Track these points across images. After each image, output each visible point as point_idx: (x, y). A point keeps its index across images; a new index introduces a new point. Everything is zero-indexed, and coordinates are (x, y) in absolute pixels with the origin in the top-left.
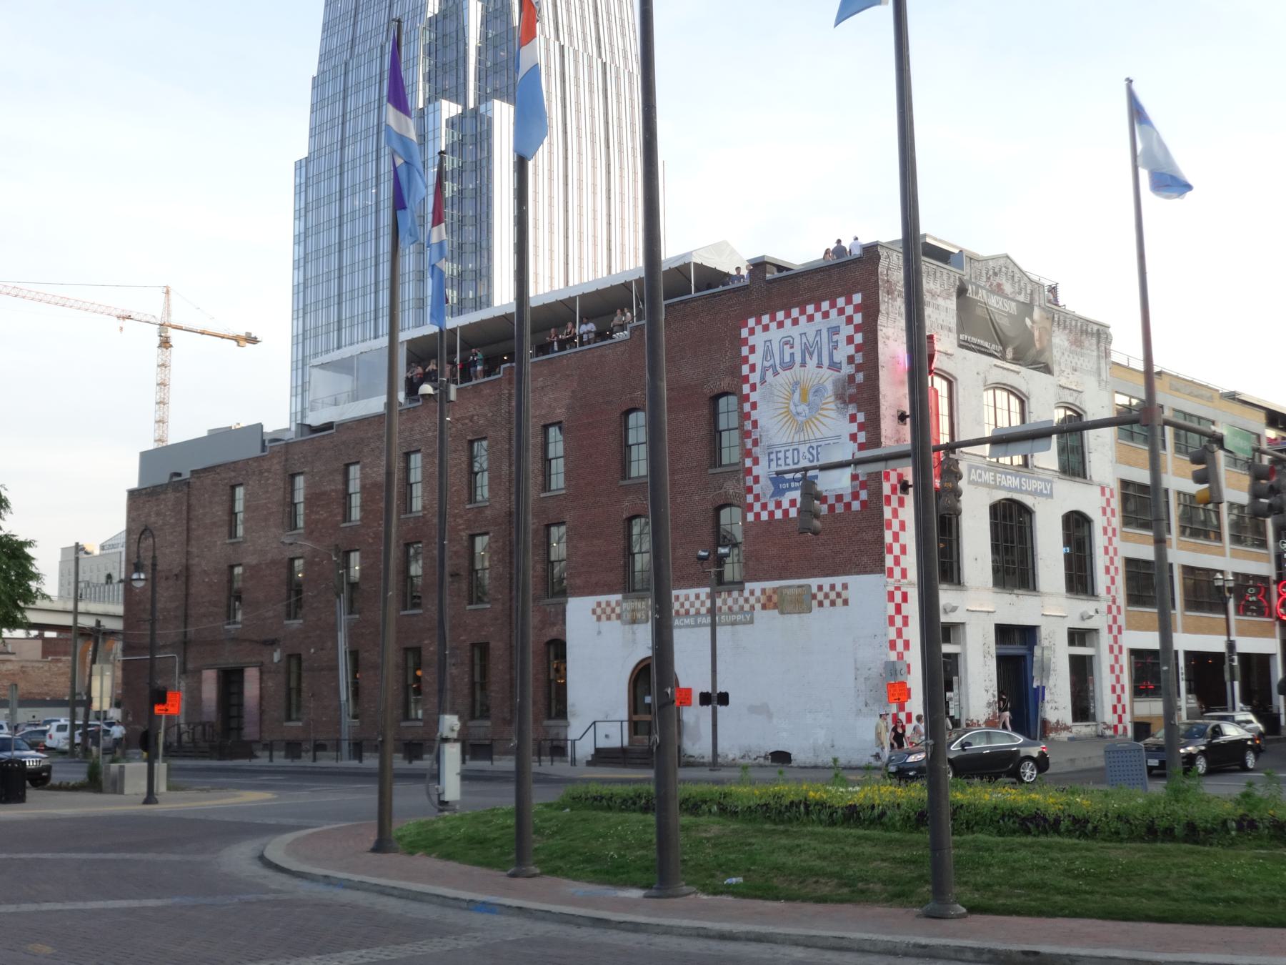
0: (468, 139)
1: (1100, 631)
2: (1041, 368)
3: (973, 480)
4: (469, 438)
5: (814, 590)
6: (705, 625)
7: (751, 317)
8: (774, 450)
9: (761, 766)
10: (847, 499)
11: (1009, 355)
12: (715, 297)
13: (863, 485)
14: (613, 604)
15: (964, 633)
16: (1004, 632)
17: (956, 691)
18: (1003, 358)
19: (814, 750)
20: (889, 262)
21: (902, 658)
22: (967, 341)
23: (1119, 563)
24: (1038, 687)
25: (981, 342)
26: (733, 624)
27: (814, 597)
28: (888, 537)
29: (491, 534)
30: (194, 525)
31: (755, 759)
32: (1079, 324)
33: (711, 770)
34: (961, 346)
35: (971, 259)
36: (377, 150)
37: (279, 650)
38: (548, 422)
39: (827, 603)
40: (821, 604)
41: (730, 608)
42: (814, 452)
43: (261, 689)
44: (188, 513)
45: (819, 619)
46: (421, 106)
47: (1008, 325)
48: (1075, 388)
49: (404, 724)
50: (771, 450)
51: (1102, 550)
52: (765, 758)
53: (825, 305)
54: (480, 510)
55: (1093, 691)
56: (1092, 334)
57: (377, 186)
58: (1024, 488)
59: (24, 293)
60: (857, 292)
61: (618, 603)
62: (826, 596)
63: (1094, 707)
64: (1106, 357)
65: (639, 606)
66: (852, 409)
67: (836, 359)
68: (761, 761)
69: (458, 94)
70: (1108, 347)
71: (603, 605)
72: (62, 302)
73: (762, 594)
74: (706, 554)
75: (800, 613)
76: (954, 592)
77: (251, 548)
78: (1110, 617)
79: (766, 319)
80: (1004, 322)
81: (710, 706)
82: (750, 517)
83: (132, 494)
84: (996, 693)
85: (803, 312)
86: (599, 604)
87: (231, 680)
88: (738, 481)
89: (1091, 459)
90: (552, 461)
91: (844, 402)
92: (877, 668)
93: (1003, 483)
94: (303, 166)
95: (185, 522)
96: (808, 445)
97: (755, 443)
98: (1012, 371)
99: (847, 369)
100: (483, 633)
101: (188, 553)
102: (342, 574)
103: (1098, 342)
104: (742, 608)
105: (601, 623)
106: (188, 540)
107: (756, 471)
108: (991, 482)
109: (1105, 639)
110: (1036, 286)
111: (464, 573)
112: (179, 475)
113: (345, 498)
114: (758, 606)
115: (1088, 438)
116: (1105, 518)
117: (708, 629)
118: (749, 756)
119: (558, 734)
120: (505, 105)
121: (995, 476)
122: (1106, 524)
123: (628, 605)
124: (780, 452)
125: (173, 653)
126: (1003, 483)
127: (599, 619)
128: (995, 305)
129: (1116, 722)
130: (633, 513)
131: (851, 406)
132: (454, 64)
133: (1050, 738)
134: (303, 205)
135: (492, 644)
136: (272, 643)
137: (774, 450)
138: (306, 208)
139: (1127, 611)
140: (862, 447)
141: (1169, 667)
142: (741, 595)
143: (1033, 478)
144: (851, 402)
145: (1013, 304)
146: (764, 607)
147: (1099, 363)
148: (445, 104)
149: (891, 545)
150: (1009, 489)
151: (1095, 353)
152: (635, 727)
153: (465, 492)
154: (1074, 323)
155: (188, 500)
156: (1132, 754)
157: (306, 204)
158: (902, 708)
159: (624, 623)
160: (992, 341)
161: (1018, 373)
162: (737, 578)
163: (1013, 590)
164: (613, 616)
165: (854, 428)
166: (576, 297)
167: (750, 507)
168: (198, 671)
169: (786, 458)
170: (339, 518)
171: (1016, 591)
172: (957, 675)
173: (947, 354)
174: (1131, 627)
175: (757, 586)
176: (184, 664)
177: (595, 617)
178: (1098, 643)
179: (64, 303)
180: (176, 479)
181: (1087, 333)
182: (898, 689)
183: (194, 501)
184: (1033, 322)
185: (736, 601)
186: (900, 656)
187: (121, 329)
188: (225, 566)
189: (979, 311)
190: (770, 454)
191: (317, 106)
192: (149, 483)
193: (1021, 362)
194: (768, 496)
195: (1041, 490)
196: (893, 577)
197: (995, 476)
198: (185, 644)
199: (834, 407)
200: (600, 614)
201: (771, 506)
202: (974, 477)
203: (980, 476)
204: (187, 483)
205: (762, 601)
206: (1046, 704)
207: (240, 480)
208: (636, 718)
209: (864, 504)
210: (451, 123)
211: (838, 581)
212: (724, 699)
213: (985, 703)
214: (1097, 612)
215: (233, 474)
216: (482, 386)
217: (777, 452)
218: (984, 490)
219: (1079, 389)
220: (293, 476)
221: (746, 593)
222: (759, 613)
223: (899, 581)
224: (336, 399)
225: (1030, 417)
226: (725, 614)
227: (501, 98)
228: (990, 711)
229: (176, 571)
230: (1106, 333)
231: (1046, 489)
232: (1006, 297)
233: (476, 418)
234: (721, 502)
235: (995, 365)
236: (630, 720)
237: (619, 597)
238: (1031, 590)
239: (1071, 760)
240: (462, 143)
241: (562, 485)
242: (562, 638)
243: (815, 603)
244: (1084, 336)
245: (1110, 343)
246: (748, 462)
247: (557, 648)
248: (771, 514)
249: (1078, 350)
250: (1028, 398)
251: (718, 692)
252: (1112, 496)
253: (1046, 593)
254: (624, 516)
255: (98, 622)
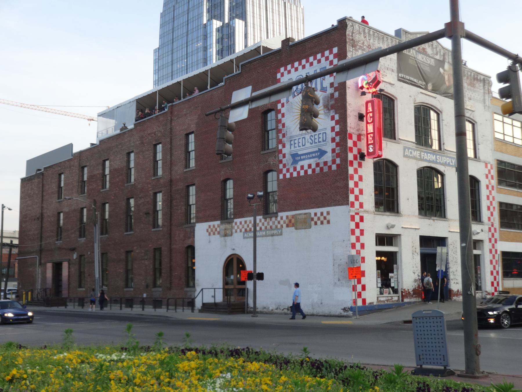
0: (225, 37)
1: (484, 241)
2: (449, 96)
3: (407, 155)
4: (154, 143)
5: (313, 215)
6: (250, 237)
7: (282, 67)
8: (293, 139)
9: (286, 314)
10: (329, 164)
11: (430, 87)
12: (265, 58)
13: (338, 155)
14: (216, 226)
15: (400, 240)
16: (425, 241)
17: (395, 273)
18: (426, 89)
19: (312, 305)
20: (353, 29)
21: (360, 253)
22: (403, 78)
23: (496, 205)
24: (439, 270)
25: (412, 79)
26: (272, 235)
27: (312, 219)
28: (351, 184)
29: (163, 192)
30: (44, 194)
31: (283, 310)
32: (472, 74)
33: (252, 316)
34: (399, 80)
35: (406, 32)
36: (187, 43)
37: (76, 253)
38: (188, 132)
39: (319, 222)
40: (316, 223)
41: (271, 227)
42: (313, 139)
43: (69, 272)
44: (43, 188)
45: (315, 231)
46: (205, 22)
47: (429, 70)
48: (470, 109)
49: (125, 290)
50: (291, 139)
51: (486, 198)
52: (288, 309)
53: (319, 56)
54: (158, 179)
55: (480, 274)
56: (480, 81)
57: (187, 58)
58: (438, 161)
59: (49, 110)
60: (335, 47)
61: (218, 226)
62: (319, 219)
63: (481, 283)
64: (489, 93)
65: (228, 227)
66: (332, 113)
67: (324, 86)
68: (286, 311)
69: (221, 17)
70: (490, 88)
71: (212, 227)
72: (65, 114)
73: (286, 219)
74: (252, 196)
75: (305, 229)
76: (394, 217)
77: (66, 204)
78: (490, 233)
79: (289, 67)
80: (427, 69)
81: (253, 281)
82: (281, 176)
83: (23, 180)
84: (420, 274)
85: (307, 61)
86: (210, 226)
87: (57, 268)
88: (275, 157)
89: (479, 148)
90: (191, 153)
91: (328, 109)
92: (345, 259)
93: (425, 158)
94: (157, 51)
95: (41, 192)
96: (310, 135)
97: (284, 136)
98: (432, 96)
99: (330, 91)
100: (159, 243)
101: (42, 207)
102: (97, 214)
103: (484, 85)
104: (276, 227)
105: (211, 237)
106: (42, 200)
107: (284, 151)
108: (418, 157)
109: (487, 246)
110: (447, 51)
111: (151, 212)
112: (40, 170)
113: (103, 177)
114: (284, 225)
115: (478, 136)
116: (487, 180)
117: (252, 240)
118: (280, 308)
119: (191, 295)
120: (241, 21)
121: (420, 154)
122: (488, 183)
123: (223, 227)
124: (296, 139)
125: (37, 255)
126: (425, 158)
127: (210, 234)
128: (421, 59)
129: (493, 291)
130: (225, 177)
131: (332, 111)
132: (219, 4)
133: (453, 300)
134: (157, 68)
135: (163, 248)
136: (73, 250)
137: (293, 139)
138: (158, 69)
139: (500, 231)
140: (279, 101)
141: (466, 244)
142: (276, 220)
143: (444, 156)
144: (331, 109)
145: (433, 60)
146: (287, 226)
147: (484, 96)
148: (214, 21)
149: (353, 189)
150: (429, 161)
151: (482, 91)
152: (226, 292)
153: (152, 172)
154: (469, 73)
155: (43, 182)
156: (432, 320)
157: (158, 67)
158: (359, 282)
159: (221, 236)
160: (419, 79)
161: (435, 98)
162: (275, 211)
163: (431, 217)
164: (216, 233)
165: (333, 123)
166: (208, 70)
167: (281, 171)
168: (45, 264)
169: (299, 143)
170: (100, 187)
171: (432, 218)
172: (396, 264)
173: (390, 84)
174: (502, 239)
175: (283, 215)
176: (40, 260)
177: (208, 233)
178: (483, 248)
179: (66, 114)
180: (38, 172)
181: (477, 80)
182: (355, 271)
183: (45, 183)
184: (444, 70)
185: (274, 223)
186: (358, 252)
187: (89, 124)
188: (56, 214)
189: (411, 62)
190: (291, 141)
191: (162, 25)
192: (27, 176)
193: (437, 92)
194: (290, 164)
195: (449, 163)
196: (354, 207)
197: (420, 154)
198: (41, 251)
199: (323, 113)
200: (210, 232)
201: (291, 170)
202: (407, 154)
203: (411, 153)
204: (42, 174)
205: (287, 223)
206: (451, 281)
207: (62, 171)
208: (226, 287)
209: (338, 166)
210: (218, 30)
211: (325, 210)
212: (261, 276)
213: (413, 279)
214: (482, 231)
215: (60, 168)
216: (159, 116)
217: (295, 140)
218: (414, 161)
219: (473, 110)
220: (83, 168)
221: (279, 219)
222: (285, 229)
223: (358, 209)
224: (107, 131)
225: (442, 122)
226: (269, 230)
227: (239, 18)
228: (416, 284)
229: (38, 216)
230: (488, 80)
231: (452, 162)
232: (428, 56)
233: (157, 132)
234: (267, 169)
235: (421, 93)
236: (224, 288)
237: (218, 222)
238: (443, 218)
239: (458, 313)
240: (222, 38)
241: (194, 165)
242: (193, 245)
243: (313, 223)
244: (476, 81)
245: (491, 86)
246: (280, 147)
247: (191, 249)
248: (291, 174)
249: (472, 88)
250: (441, 112)
251: (257, 272)
252: (492, 168)
253: (451, 220)
254: (222, 179)
255: (12, 241)
